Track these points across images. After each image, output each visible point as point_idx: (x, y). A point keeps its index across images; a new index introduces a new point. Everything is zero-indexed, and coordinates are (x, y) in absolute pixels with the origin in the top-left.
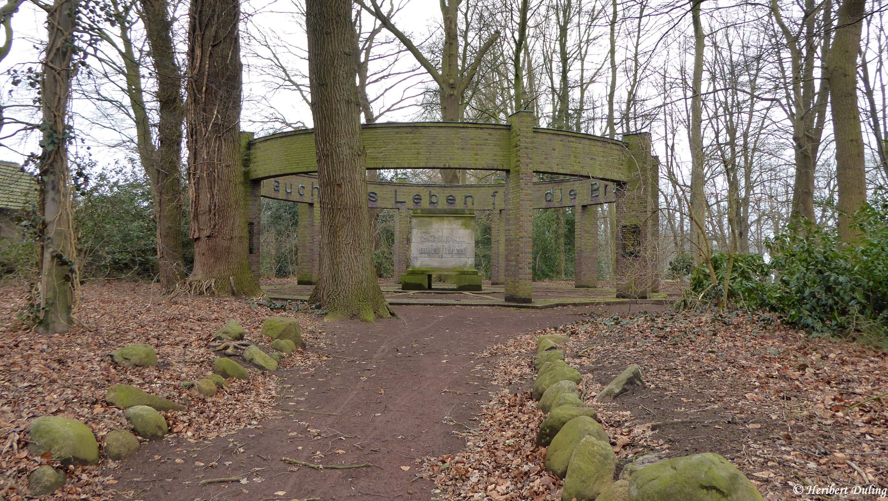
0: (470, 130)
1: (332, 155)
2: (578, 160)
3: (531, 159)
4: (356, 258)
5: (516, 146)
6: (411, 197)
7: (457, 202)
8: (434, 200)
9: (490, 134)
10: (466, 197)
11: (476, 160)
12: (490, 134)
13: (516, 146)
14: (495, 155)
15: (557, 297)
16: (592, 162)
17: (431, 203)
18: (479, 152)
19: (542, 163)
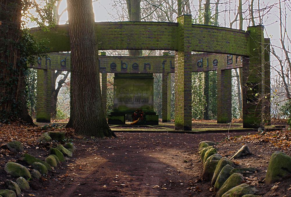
0: (153, 26)
1: (80, 45)
2: (219, 43)
3: (190, 44)
4: (93, 103)
5: (182, 36)
6: (109, 65)
7: (140, 68)
8: (124, 67)
9: (165, 29)
10: (145, 65)
11: (158, 44)
12: (165, 29)
13: (182, 36)
14: (169, 41)
15: (207, 128)
16: (227, 44)
17: (122, 68)
18: (159, 40)
19: (197, 46)
